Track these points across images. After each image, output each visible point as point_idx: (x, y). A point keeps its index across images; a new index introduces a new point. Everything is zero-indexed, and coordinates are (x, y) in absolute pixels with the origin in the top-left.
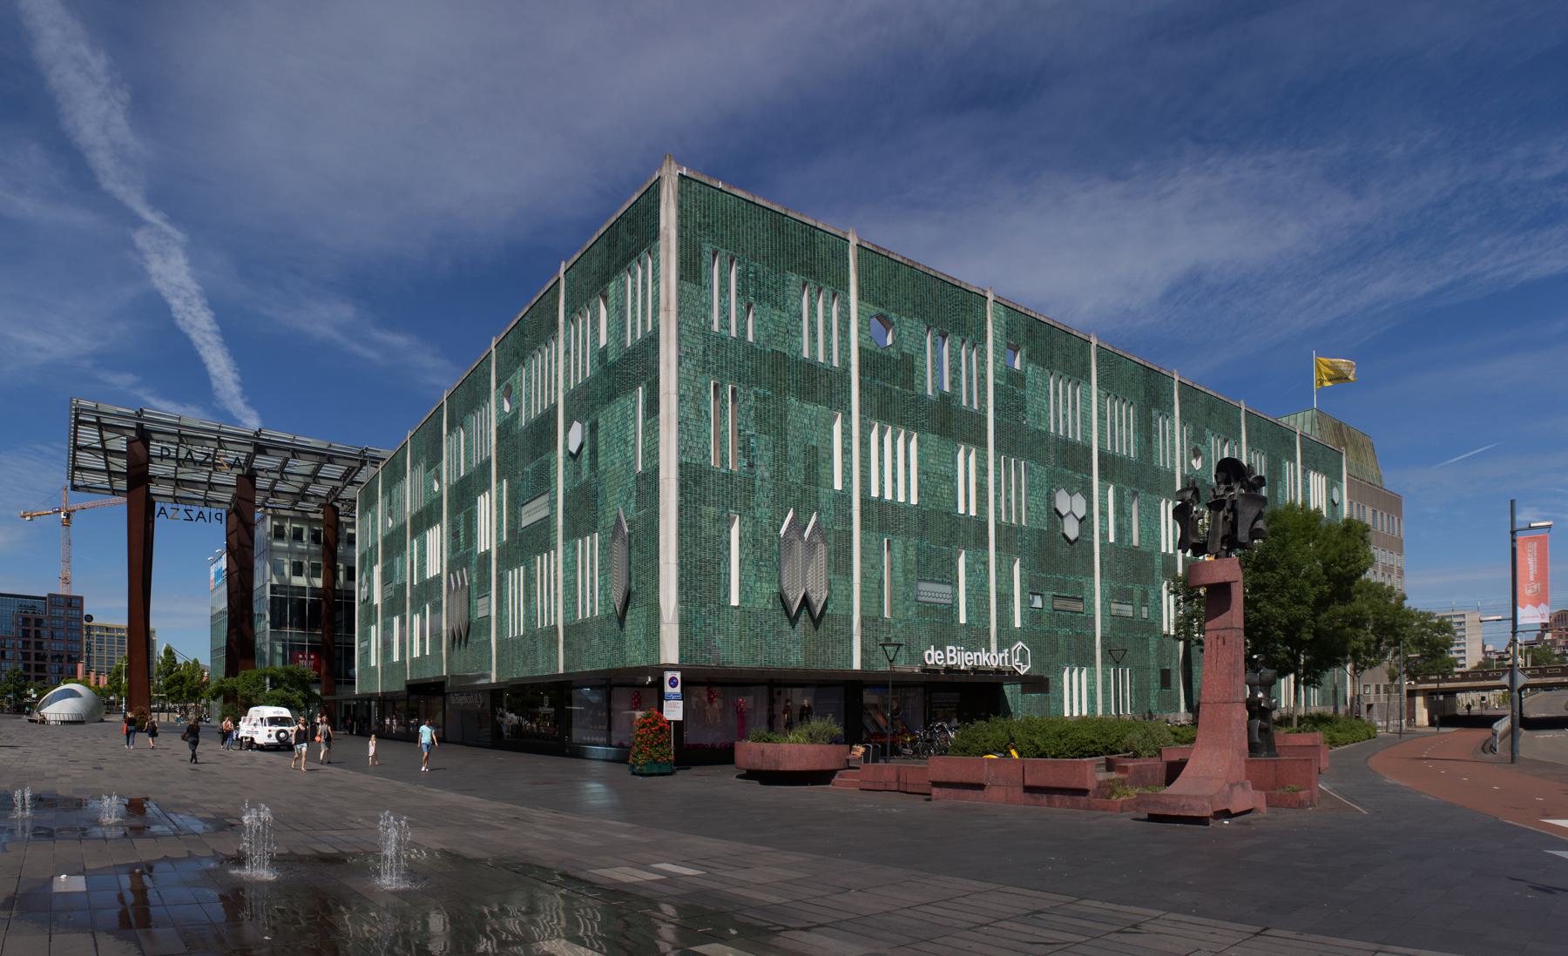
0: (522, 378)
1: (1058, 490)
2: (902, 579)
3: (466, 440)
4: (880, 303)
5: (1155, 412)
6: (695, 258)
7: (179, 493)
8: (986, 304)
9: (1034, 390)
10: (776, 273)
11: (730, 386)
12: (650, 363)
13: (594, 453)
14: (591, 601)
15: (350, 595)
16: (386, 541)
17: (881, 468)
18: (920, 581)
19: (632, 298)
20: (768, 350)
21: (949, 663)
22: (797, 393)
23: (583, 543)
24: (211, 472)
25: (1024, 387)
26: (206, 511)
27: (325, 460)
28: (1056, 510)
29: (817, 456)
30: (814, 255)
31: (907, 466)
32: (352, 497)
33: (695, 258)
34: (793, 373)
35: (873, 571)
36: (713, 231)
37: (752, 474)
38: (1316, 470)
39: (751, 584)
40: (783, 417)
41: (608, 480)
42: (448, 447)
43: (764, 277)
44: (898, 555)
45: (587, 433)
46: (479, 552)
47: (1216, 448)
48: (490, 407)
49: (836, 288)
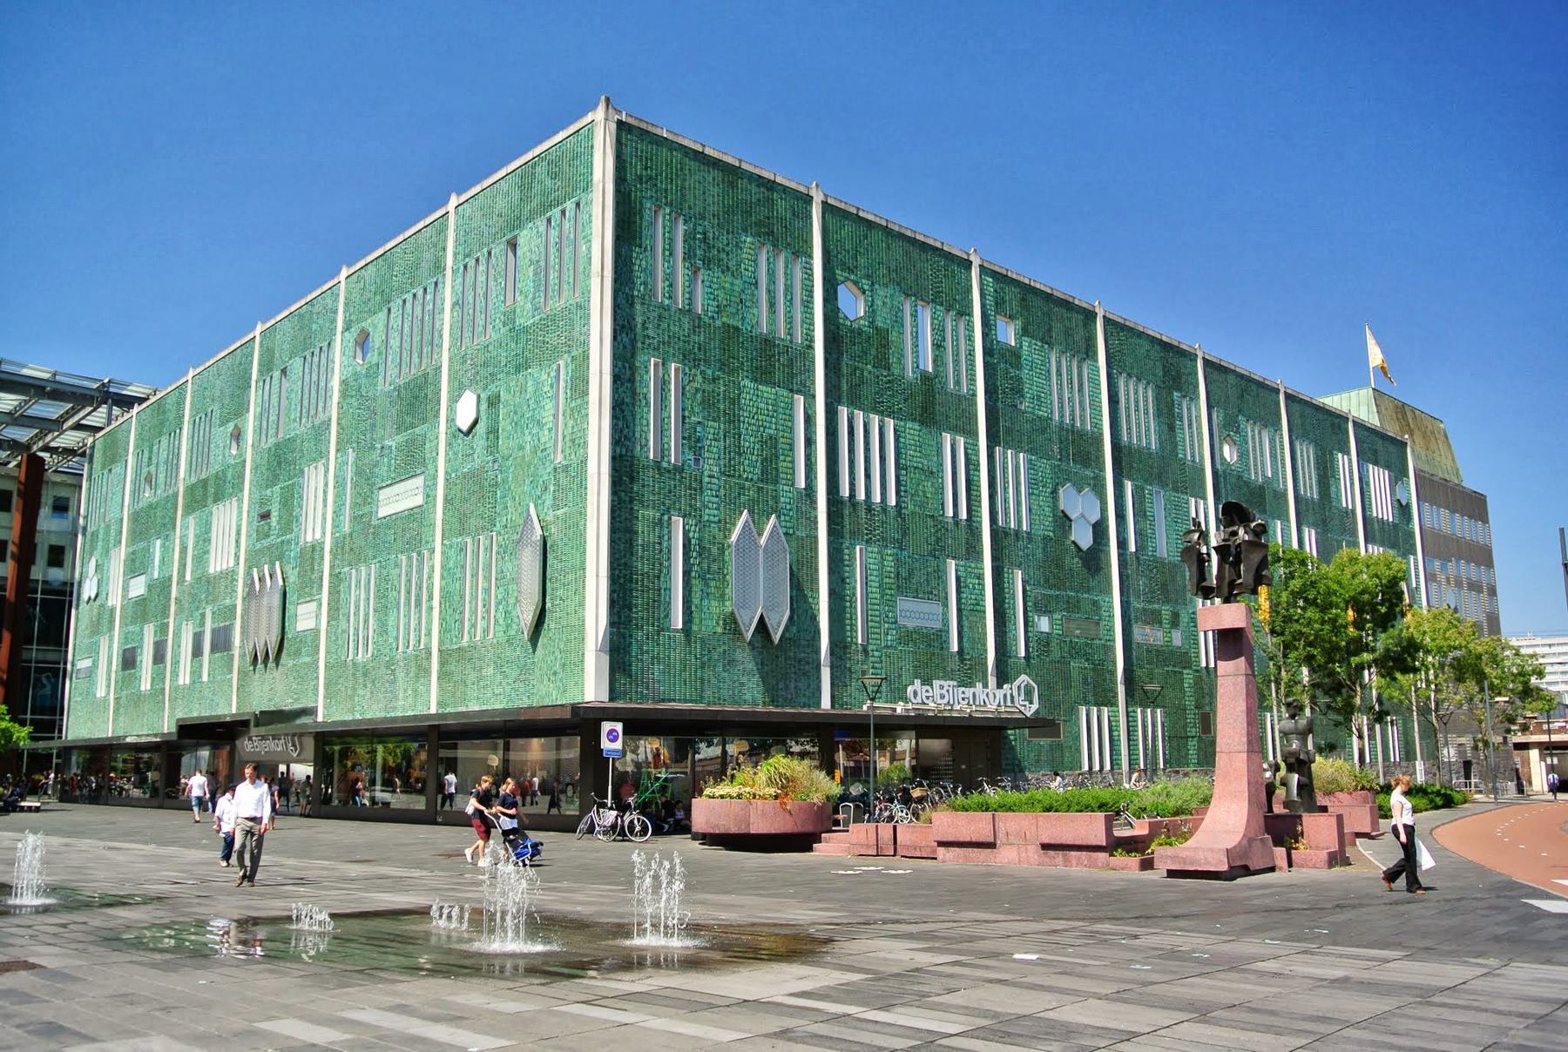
10: (728, 233)
12: (576, 334)
13: (493, 432)
16: (135, 517)
17: (852, 450)
25: (1019, 366)
36: (656, 185)
38: (1376, 463)
40: (735, 401)
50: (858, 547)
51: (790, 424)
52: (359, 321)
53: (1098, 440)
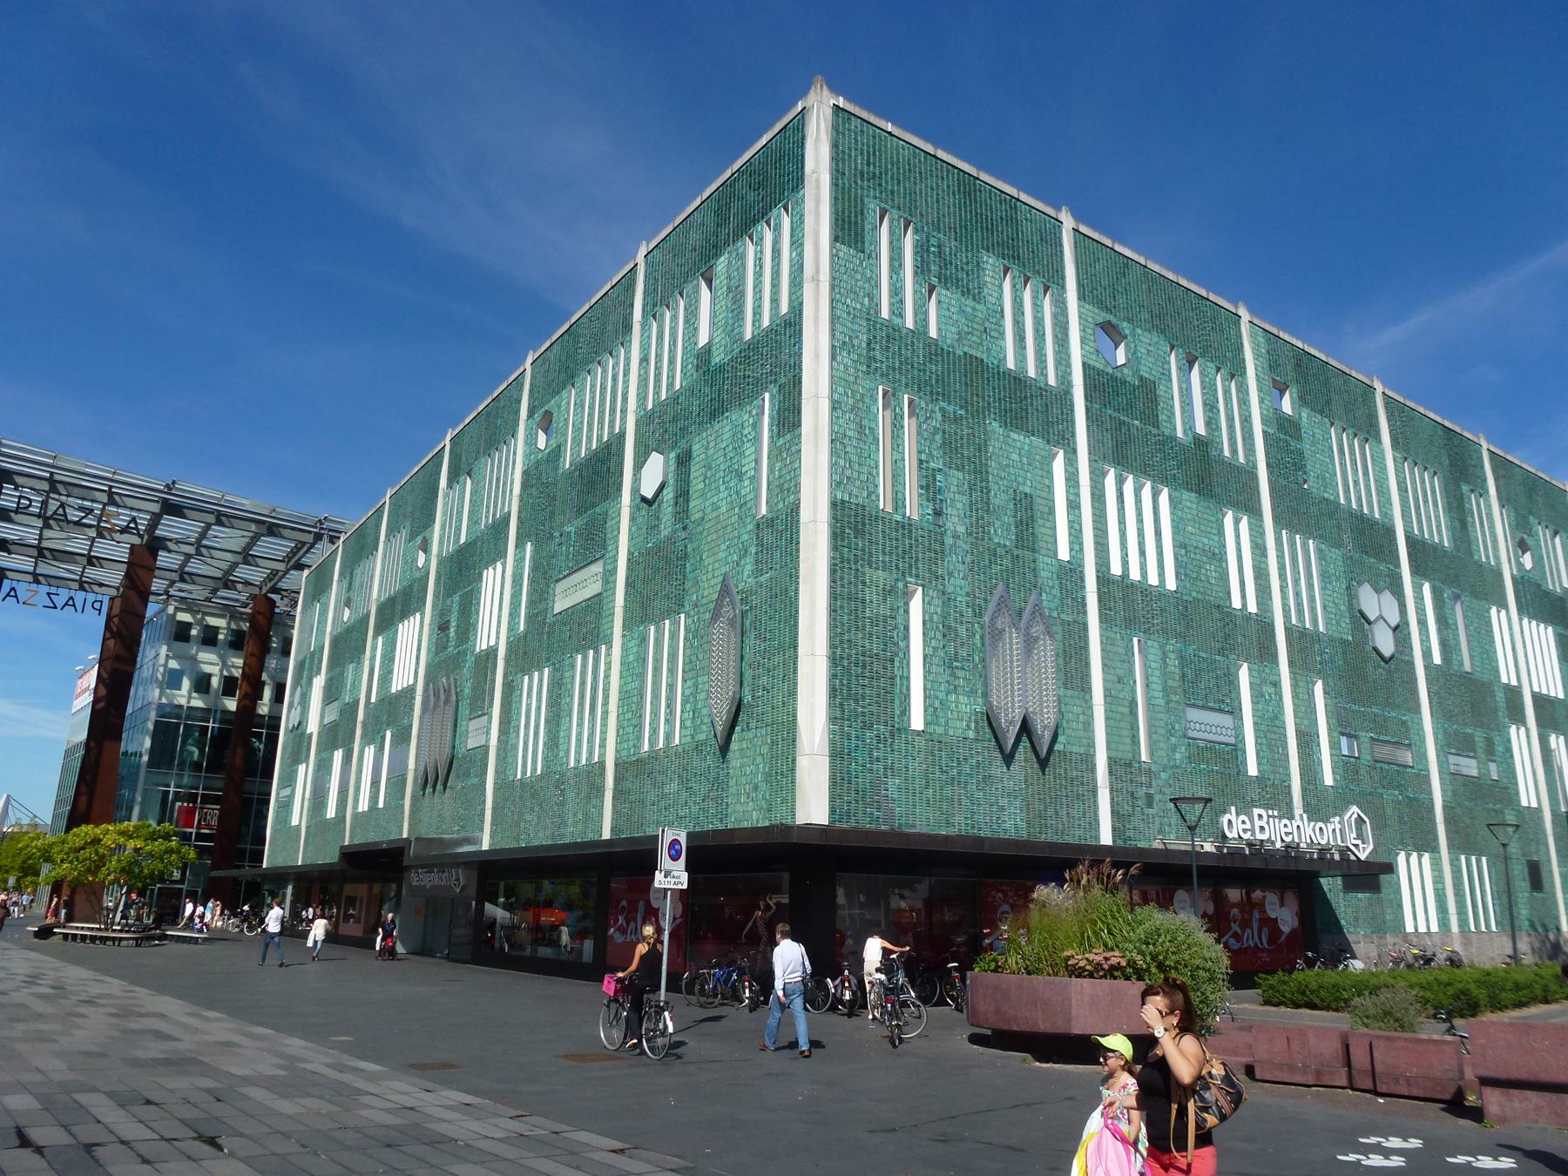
0: (568, 403)
1: (1360, 583)
2: (1162, 702)
3: (474, 493)
4: (1106, 307)
5: (1465, 488)
6: (856, 216)
7: (43, 569)
8: (1239, 324)
9: (1313, 444)
10: (967, 251)
11: (906, 396)
13: (683, 495)
14: (667, 721)
15: (274, 722)
16: (335, 642)
18: (1188, 705)
19: (755, 273)
20: (959, 352)
21: (1259, 836)
22: (1000, 416)
23: (657, 631)
24: (93, 540)
25: (1299, 438)
26: (80, 597)
27: (264, 529)
28: (1361, 612)
29: (1032, 509)
30: (1018, 235)
31: (1158, 533)
32: (294, 588)
33: (856, 216)
34: (994, 389)
35: (1119, 686)
36: (880, 185)
37: (940, 527)
39: (941, 695)
40: (981, 448)
41: (705, 534)
42: (445, 505)
43: (950, 254)
44: (1154, 665)
45: (672, 468)
46: (478, 650)
47: (1546, 541)
48: (515, 445)
49: (1048, 281)
50: (1135, 640)
51: (1047, 482)
52: (543, 404)
53: (1390, 532)
